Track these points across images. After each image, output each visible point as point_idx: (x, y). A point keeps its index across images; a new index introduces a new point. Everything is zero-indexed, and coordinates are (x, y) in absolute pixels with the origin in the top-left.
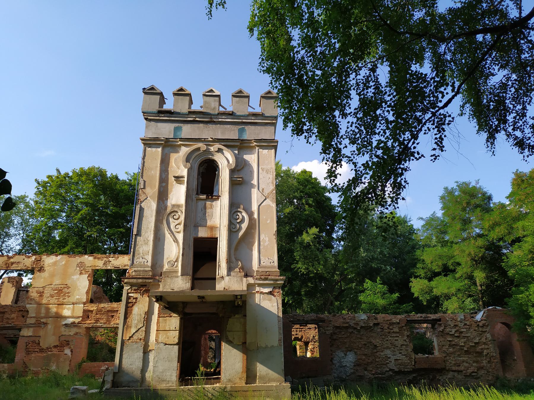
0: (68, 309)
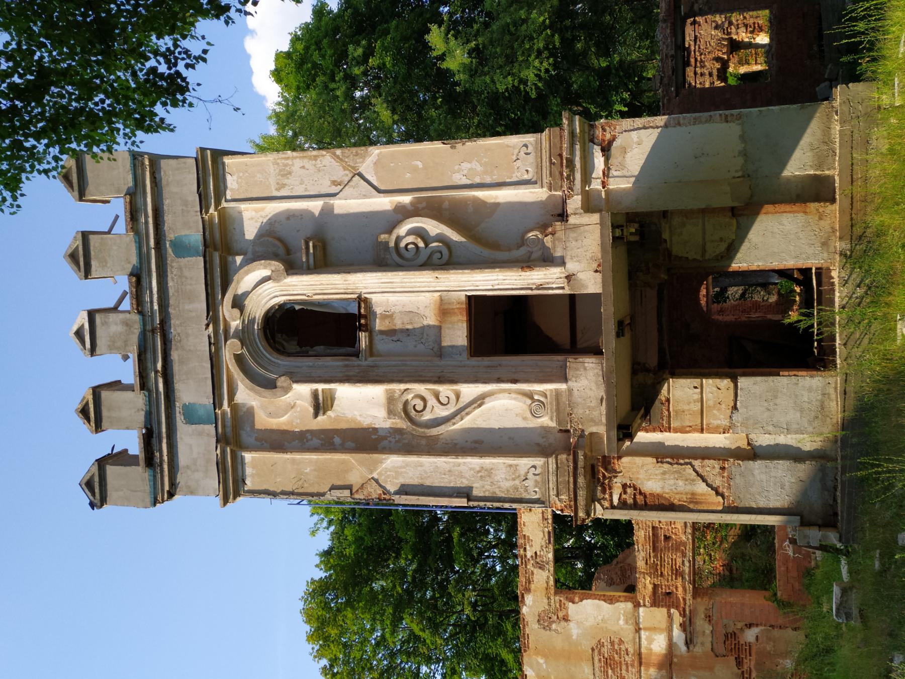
0: (650, 641)
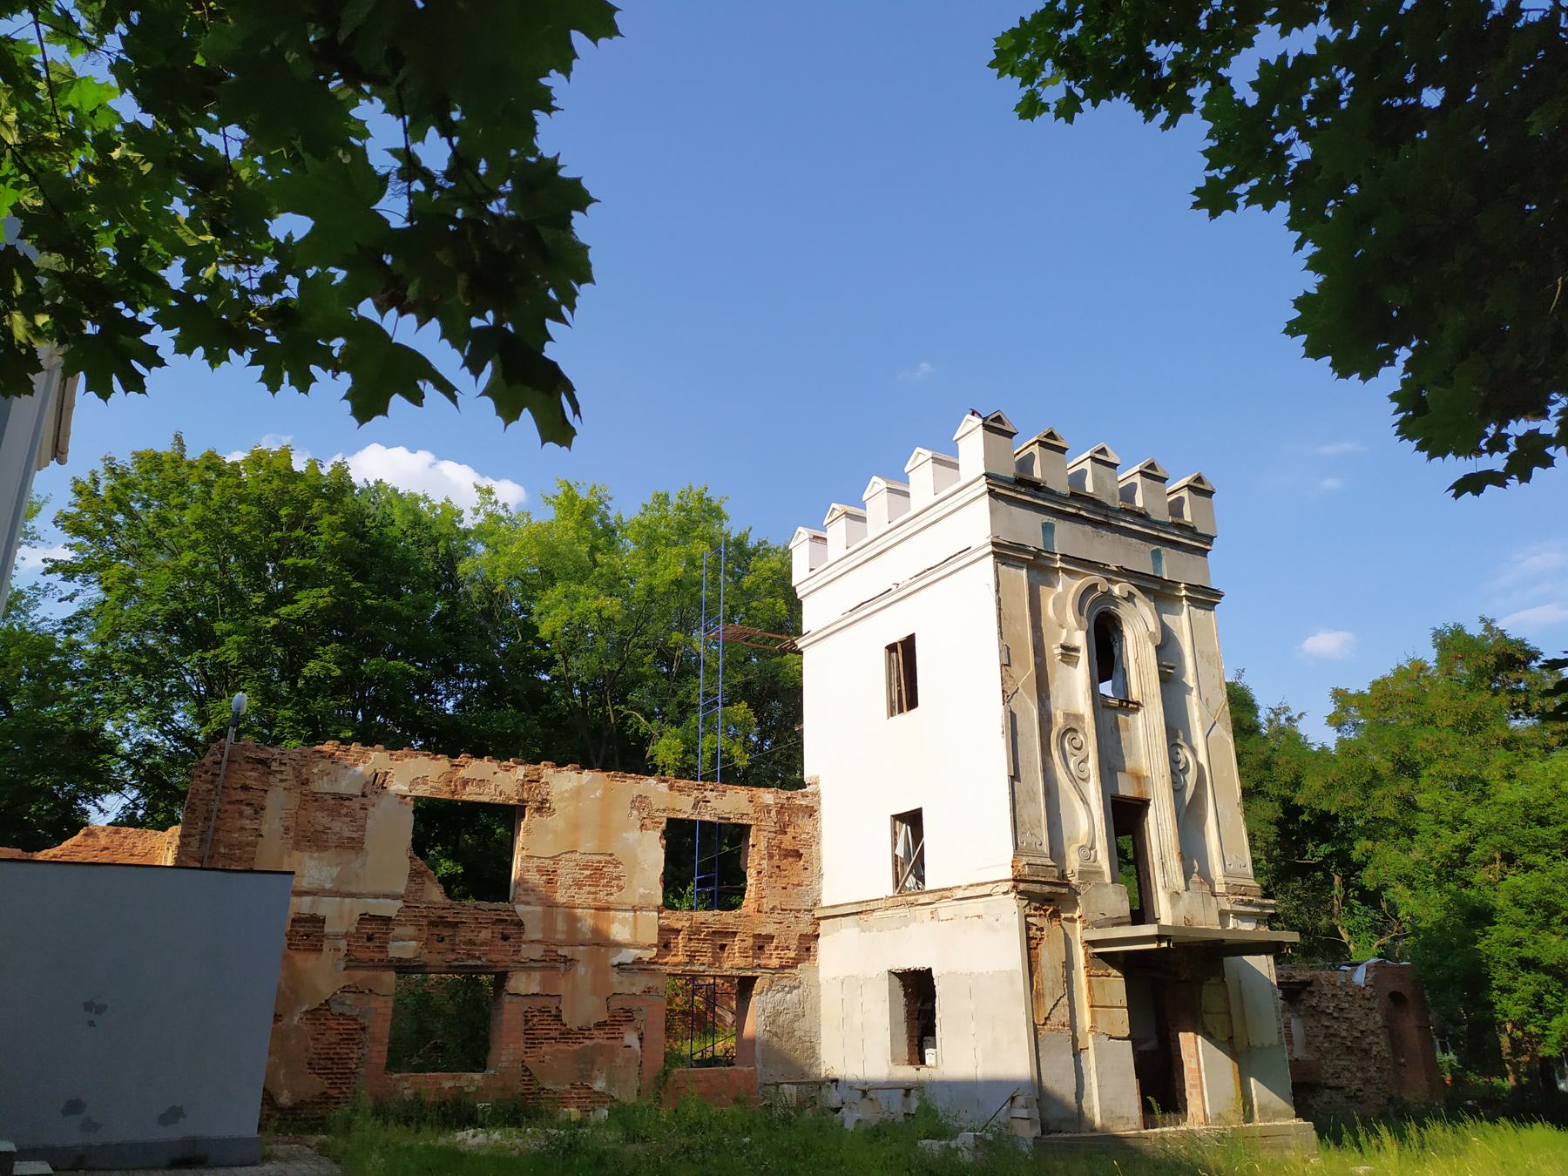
0: (623, 922)
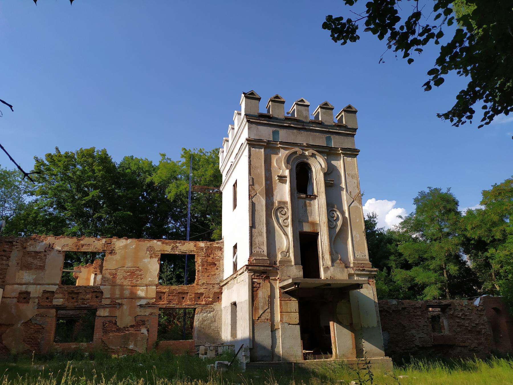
0: (142, 290)
